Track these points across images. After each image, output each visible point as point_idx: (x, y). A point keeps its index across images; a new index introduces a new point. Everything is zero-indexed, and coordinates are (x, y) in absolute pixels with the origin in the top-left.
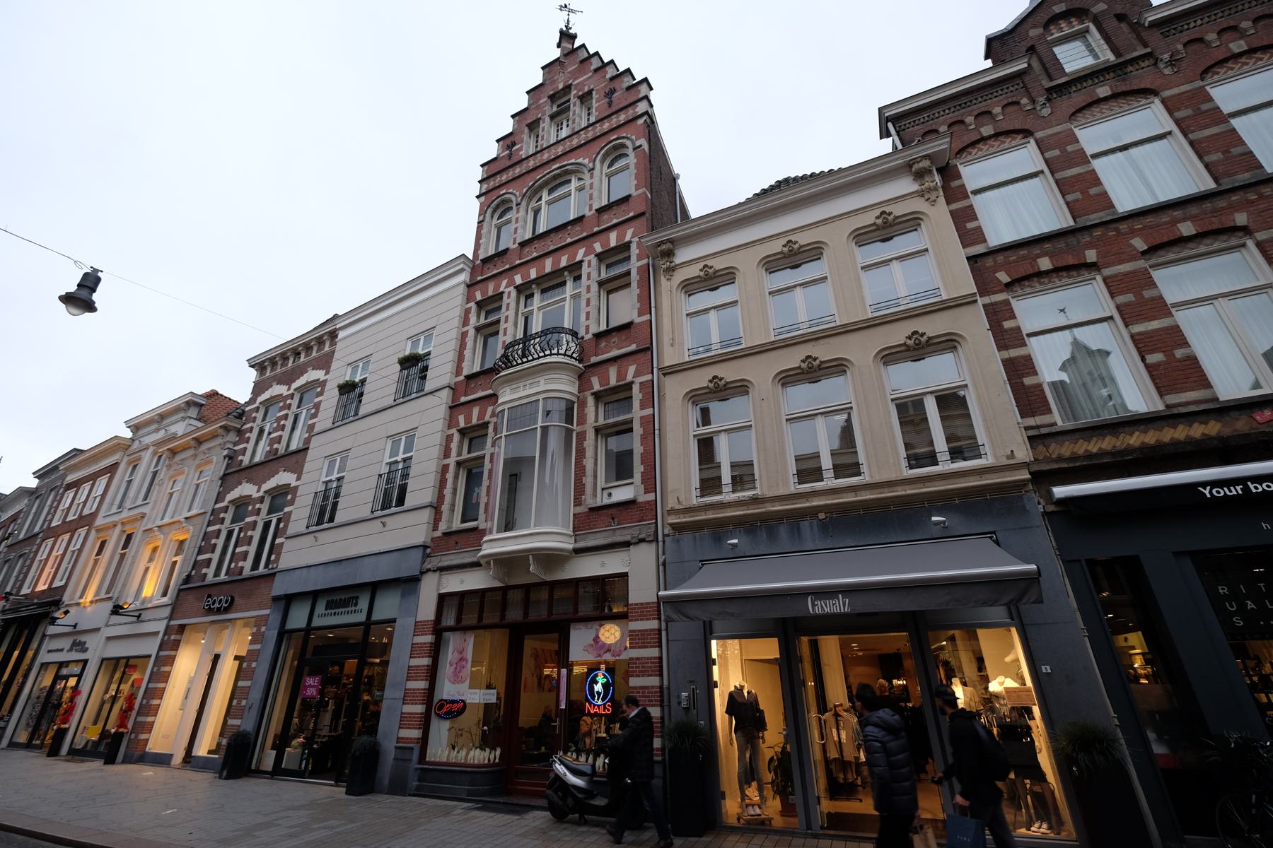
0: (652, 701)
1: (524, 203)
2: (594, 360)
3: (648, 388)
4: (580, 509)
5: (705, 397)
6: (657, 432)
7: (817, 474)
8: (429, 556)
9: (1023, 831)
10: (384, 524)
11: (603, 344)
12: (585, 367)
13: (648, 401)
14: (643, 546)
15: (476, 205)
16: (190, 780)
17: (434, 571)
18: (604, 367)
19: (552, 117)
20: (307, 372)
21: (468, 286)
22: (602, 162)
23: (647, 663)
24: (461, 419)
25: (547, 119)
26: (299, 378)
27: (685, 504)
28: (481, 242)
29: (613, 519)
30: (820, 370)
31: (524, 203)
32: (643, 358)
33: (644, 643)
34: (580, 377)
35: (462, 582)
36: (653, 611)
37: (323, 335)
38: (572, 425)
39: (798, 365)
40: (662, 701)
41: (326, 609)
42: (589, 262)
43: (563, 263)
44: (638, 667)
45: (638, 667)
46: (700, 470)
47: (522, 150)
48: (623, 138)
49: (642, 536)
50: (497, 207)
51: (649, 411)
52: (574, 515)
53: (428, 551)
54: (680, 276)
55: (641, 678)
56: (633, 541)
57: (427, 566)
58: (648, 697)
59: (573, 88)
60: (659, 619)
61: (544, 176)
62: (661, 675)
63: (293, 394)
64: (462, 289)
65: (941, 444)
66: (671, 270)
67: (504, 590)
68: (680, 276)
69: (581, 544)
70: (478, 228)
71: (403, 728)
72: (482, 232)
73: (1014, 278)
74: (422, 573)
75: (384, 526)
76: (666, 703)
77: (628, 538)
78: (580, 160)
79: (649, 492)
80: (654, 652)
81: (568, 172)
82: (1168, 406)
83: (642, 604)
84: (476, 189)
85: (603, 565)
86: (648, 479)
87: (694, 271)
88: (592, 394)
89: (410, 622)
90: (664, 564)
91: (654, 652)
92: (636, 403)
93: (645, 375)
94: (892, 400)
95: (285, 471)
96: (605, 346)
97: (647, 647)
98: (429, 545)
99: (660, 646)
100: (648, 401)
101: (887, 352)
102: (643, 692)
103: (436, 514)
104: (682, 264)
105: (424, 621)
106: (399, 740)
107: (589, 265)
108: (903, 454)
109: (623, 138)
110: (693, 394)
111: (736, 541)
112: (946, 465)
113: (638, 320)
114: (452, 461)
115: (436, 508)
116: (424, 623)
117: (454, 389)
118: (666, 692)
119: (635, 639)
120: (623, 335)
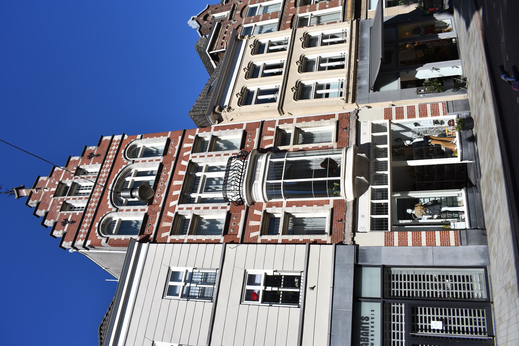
0: (424, 107)
7: (341, 93)
17: (354, 235)
23: (409, 110)
33: (401, 112)
36: (403, 234)
39: (302, 43)
44: (411, 113)
45: (411, 113)
46: (325, 226)
55: (416, 112)
58: (423, 109)
71: (450, 243)
73: (291, 19)
82: (342, 5)
83: (385, 114)
89: (386, 250)
97: (403, 111)
106: (457, 245)
119: (400, 109)
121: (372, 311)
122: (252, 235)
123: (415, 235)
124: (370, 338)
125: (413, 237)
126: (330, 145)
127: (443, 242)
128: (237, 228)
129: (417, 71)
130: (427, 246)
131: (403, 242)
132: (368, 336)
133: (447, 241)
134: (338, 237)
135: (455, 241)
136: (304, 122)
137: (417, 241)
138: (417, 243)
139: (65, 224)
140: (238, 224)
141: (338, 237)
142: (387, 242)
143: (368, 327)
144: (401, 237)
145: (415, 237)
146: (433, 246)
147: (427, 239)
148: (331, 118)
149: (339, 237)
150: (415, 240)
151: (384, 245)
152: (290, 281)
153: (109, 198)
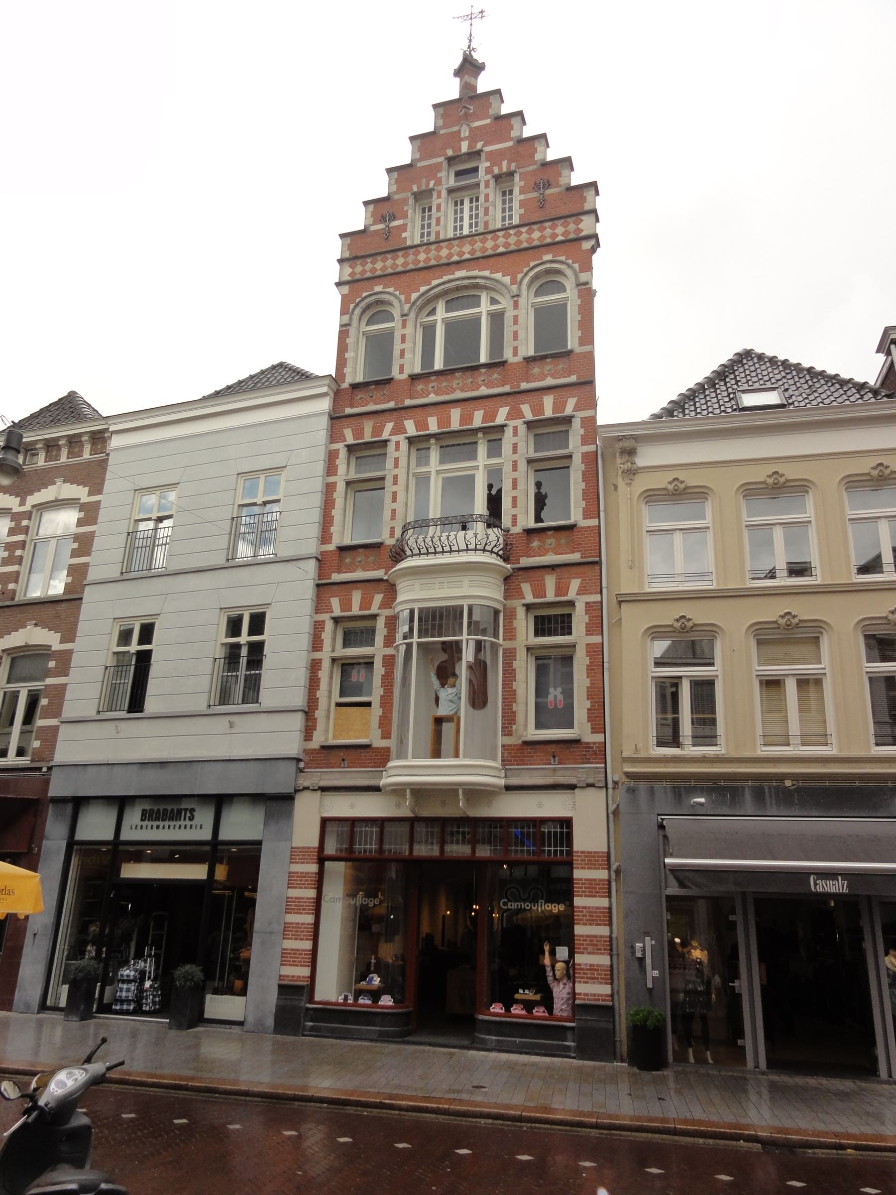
1: (412, 315)
2: (525, 562)
3: (595, 611)
4: (509, 741)
5: (668, 634)
6: (606, 665)
8: (301, 771)
9: (497, 1008)
10: (231, 725)
11: (348, 560)
12: (513, 569)
13: (595, 625)
14: (591, 790)
15: (335, 298)
16: (104, 1041)
18: (538, 573)
19: (450, 191)
20: (54, 483)
21: (332, 418)
22: (529, 286)
24: (335, 603)
25: (444, 193)
26: (39, 490)
27: (642, 755)
28: (347, 355)
29: (554, 757)
30: (797, 628)
31: (412, 315)
32: (589, 571)
34: (507, 579)
35: (352, 806)
37: (59, 438)
38: (498, 639)
39: (671, 623)
40: (611, 950)
41: (142, 820)
42: (515, 429)
43: (478, 420)
47: (405, 230)
48: (562, 262)
49: (590, 781)
50: (368, 307)
51: (596, 639)
52: (503, 746)
53: (302, 765)
54: (644, 483)
56: (581, 784)
57: (303, 782)
59: (483, 155)
60: (609, 868)
61: (444, 283)
62: (610, 924)
63: (30, 513)
64: (324, 421)
65: (794, 728)
66: (632, 473)
67: (412, 821)
68: (644, 483)
69: (514, 781)
70: (340, 332)
72: (348, 341)
74: (297, 791)
75: (231, 727)
76: (614, 952)
77: (573, 781)
78: (498, 276)
79: (596, 732)
80: (603, 902)
81: (476, 286)
84: (334, 272)
85: (540, 805)
86: (596, 717)
87: (661, 481)
88: (524, 605)
90: (616, 813)
91: (603, 902)
92: (379, 639)
93: (592, 593)
94: (867, 673)
95: (36, 625)
96: (539, 548)
98: (301, 757)
99: (610, 897)
100: (595, 625)
101: (869, 622)
102: (591, 941)
103: (307, 720)
104: (645, 468)
105: (304, 848)
107: (515, 433)
108: (759, 731)
109: (562, 262)
110: (655, 630)
111: (702, 800)
112: (690, 750)
113: (583, 523)
114: (325, 656)
115: (309, 713)
116: (305, 850)
117: (321, 561)
118: (614, 942)
120: (563, 537)
121: (201, 825)
122: (335, 603)
123: (306, 902)
124: (167, 823)
125: (303, 898)
126: (516, 729)
127: (290, 954)
128: (542, 552)
129: (582, 220)
130: (285, 923)
131: (297, 880)
132: (169, 820)
133: (290, 961)
134: (318, 760)
135: (288, 976)
136: (588, 663)
137: (295, 906)
138: (291, 905)
139: (381, 222)
140: (360, 569)
141: (318, 760)
142: (300, 852)
143: (180, 820)
144: (305, 877)
145: (304, 902)
146: (284, 935)
147: (297, 924)
148: (592, 725)
149: (318, 764)
150: (299, 902)
151: (294, 845)
152: (253, 687)
153: (435, 282)
